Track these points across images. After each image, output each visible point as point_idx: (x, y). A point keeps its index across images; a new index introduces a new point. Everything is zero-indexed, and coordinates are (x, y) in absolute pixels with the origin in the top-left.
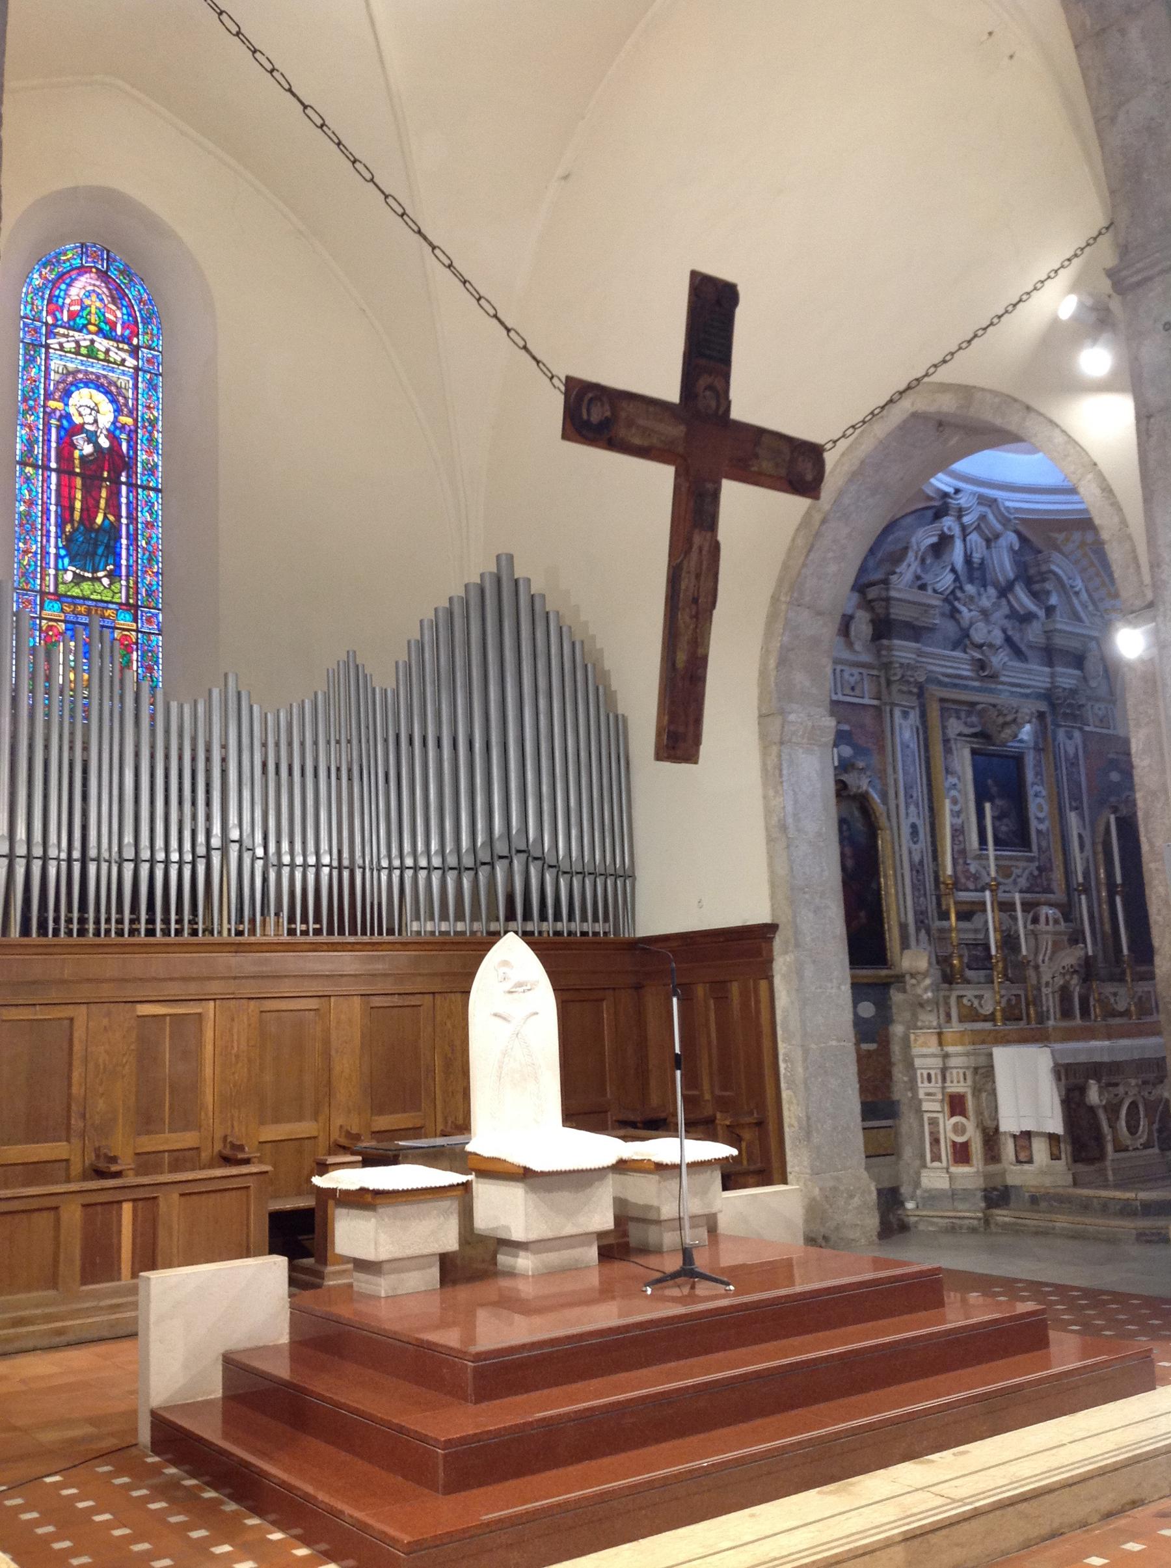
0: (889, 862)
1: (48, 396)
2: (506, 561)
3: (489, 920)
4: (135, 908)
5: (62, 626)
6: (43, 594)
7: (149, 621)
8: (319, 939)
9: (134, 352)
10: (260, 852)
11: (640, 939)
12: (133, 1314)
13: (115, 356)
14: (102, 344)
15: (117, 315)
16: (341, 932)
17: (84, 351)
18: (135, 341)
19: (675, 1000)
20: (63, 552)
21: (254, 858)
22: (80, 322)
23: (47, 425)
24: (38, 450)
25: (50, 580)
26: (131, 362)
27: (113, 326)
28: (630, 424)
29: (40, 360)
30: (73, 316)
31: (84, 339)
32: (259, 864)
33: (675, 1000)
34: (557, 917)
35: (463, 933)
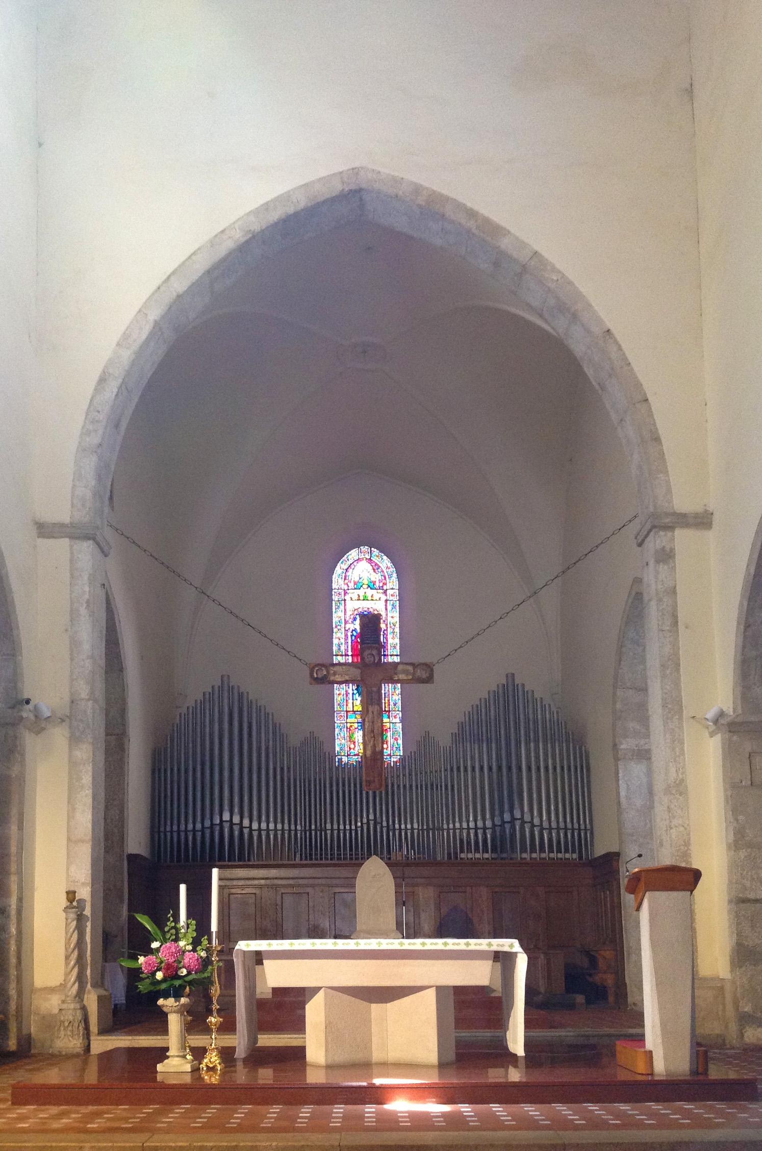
0: (13, 859)
1: (346, 622)
2: (511, 677)
3: (549, 852)
4: (339, 847)
5: (356, 725)
6: (347, 712)
7: (395, 717)
8: (333, 862)
9: (385, 592)
10: (385, 824)
11: (600, 857)
12: (465, 1034)
13: (376, 597)
14: (370, 592)
15: (376, 577)
16: (321, 859)
17: (361, 598)
18: (385, 588)
20: (355, 692)
21: (382, 827)
22: (359, 585)
23: (346, 636)
24: (343, 648)
25: (350, 705)
26: (384, 598)
27: (374, 583)
28: (335, 674)
29: (342, 607)
30: (355, 583)
31: (361, 592)
32: (385, 830)
34: (542, 849)
35: (487, 859)
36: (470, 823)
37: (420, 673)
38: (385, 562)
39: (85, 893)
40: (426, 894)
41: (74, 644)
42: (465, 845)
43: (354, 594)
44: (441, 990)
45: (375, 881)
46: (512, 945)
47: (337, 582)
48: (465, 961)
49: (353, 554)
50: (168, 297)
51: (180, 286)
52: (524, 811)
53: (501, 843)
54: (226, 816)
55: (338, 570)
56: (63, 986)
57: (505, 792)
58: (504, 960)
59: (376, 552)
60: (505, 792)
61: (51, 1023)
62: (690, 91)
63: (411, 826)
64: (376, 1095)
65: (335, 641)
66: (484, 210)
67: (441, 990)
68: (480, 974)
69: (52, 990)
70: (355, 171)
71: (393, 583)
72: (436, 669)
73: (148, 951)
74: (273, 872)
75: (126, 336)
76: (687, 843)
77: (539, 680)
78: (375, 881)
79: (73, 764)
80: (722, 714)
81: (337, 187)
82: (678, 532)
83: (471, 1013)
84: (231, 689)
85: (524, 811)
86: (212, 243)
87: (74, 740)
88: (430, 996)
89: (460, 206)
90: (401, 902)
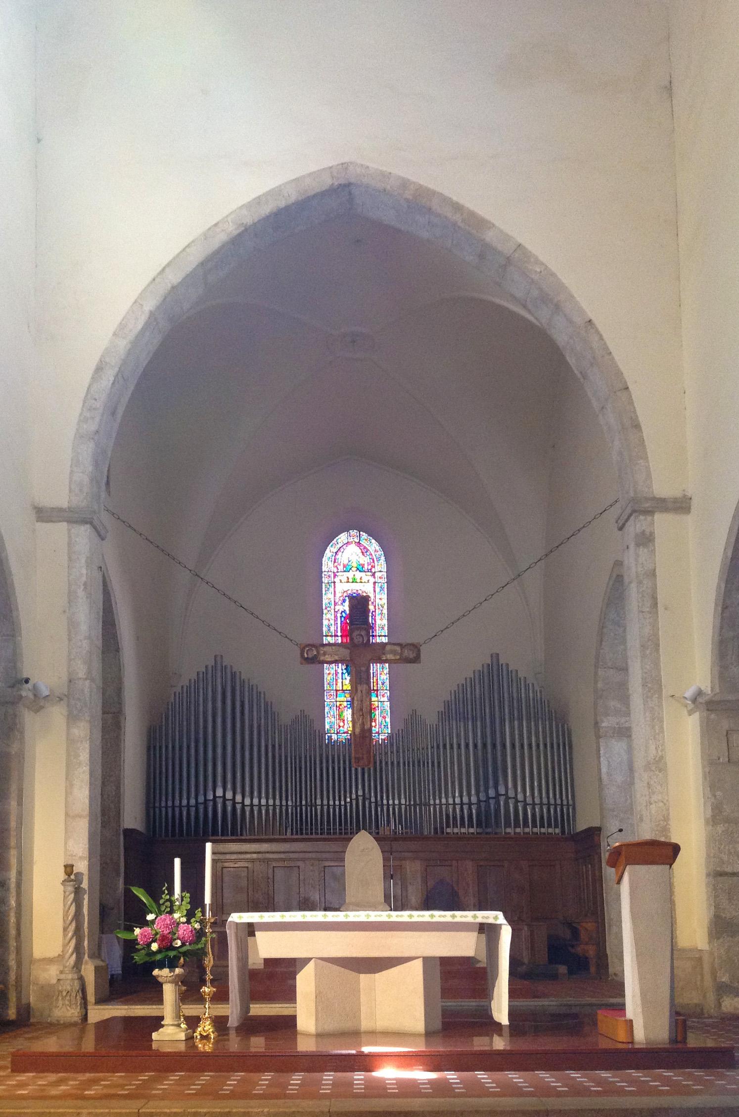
0: (13, 833)
1: (335, 604)
2: (496, 657)
3: (533, 827)
4: (329, 822)
5: (345, 704)
6: (337, 691)
7: (383, 696)
8: (323, 836)
9: (373, 575)
10: (373, 799)
11: (582, 832)
12: (451, 1004)
13: (365, 579)
14: (358, 575)
15: (365, 560)
16: (312, 834)
17: (351, 580)
18: (373, 570)
19: (177, 862)
20: (345, 671)
21: (370, 803)
22: (348, 568)
23: (336, 617)
24: (332, 629)
25: (340, 684)
26: (372, 580)
27: (363, 566)
29: (332, 589)
30: (344, 566)
31: (350, 575)
32: (373, 805)
33: (177, 862)
34: (526, 824)
35: (473, 833)
36: (456, 799)
37: (407, 653)
38: (373, 546)
39: (82, 867)
40: (413, 868)
41: (72, 625)
42: (451, 820)
43: (343, 576)
44: (428, 961)
45: (364, 855)
46: (496, 917)
47: (327, 564)
48: (451, 932)
49: (343, 538)
50: (163, 288)
51: (174, 278)
52: (508, 787)
53: (486, 818)
54: (219, 792)
55: (328, 553)
56: (61, 957)
57: (490, 768)
58: (489, 931)
59: (364, 535)
60: (490, 768)
61: (49, 993)
62: (669, 88)
63: (398, 801)
64: (365, 1063)
65: (325, 622)
66: (470, 204)
67: (428, 961)
68: (465, 945)
69: (50, 961)
70: (345, 166)
71: (381, 566)
72: (423, 649)
73: (144, 923)
74: (265, 847)
75: (122, 326)
76: (666, 819)
77: (522, 660)
78: (364, 855)
79: (71, 741)
80: (700, 693)
81: (327, 182)
82: (657, 516)
83: (457, 983)
84: (224, 669)
85: (508, 787)
86: (206, 236)
87: (72, 718)
88: (417, 967)
89: (446, 200)
90: (388, 875)
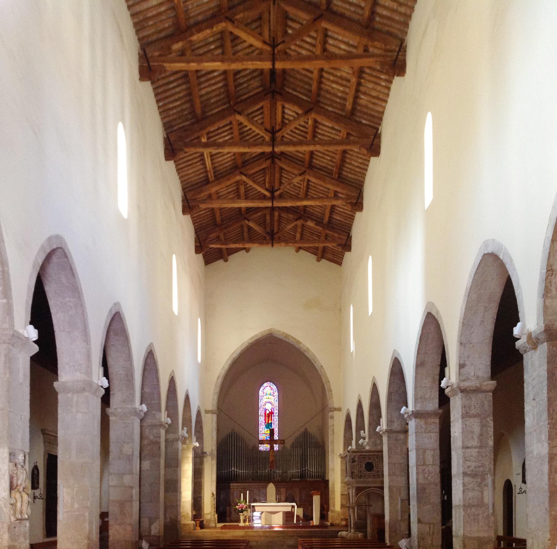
2: (306, 429)
15: (272, 392)
31: (267, 396)
36: (294, 471)
37: (282, 442)
38: (274, 387)
39: (215, 493)
40: (283, 490)
41: (212, 437)
42: (293, 477)
43: (265, 397)
44: (283, 512)
45: (271, 489)
46: (294, 504)
47: (261, 393)
48: (287, 507)
49: (265, 384)
50: (232, 358)
51: (235, 356)
52: (308, 468)
53: (302, 476)
54: (233, 469)
55: (261, 389)
56: (210, 513)
57: (304, 461)
58: (293, 507)
59: (272, 384)
60: (304, 461)
61: (209, 521)
62: (340, 310)
63: (279, 472)
64: (273, 527)
65: (260, 412)
66: (297, 338)
67: (283, 512)
68: (289, 509)
69: (208, 514)
70: (271, 329)
71: (276, 394)
72: (286, 441)
73: (237, 505)
74: (245, 484)
75: (223, 367)
76: (334, 482)
77: (313, 430)
78: (271, 489)
79: (212, 464)
80: (341, 454)
81: (267, 333)
82: (335, 412)
83: (288, 516)
84: (234, 433)
85: (308, 468)
86: (241, 346)
87: (212, 459)
88: (281, 514)
89: (292, 337)
90: (277, 494)
